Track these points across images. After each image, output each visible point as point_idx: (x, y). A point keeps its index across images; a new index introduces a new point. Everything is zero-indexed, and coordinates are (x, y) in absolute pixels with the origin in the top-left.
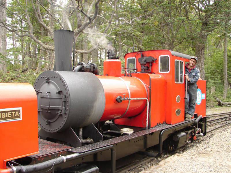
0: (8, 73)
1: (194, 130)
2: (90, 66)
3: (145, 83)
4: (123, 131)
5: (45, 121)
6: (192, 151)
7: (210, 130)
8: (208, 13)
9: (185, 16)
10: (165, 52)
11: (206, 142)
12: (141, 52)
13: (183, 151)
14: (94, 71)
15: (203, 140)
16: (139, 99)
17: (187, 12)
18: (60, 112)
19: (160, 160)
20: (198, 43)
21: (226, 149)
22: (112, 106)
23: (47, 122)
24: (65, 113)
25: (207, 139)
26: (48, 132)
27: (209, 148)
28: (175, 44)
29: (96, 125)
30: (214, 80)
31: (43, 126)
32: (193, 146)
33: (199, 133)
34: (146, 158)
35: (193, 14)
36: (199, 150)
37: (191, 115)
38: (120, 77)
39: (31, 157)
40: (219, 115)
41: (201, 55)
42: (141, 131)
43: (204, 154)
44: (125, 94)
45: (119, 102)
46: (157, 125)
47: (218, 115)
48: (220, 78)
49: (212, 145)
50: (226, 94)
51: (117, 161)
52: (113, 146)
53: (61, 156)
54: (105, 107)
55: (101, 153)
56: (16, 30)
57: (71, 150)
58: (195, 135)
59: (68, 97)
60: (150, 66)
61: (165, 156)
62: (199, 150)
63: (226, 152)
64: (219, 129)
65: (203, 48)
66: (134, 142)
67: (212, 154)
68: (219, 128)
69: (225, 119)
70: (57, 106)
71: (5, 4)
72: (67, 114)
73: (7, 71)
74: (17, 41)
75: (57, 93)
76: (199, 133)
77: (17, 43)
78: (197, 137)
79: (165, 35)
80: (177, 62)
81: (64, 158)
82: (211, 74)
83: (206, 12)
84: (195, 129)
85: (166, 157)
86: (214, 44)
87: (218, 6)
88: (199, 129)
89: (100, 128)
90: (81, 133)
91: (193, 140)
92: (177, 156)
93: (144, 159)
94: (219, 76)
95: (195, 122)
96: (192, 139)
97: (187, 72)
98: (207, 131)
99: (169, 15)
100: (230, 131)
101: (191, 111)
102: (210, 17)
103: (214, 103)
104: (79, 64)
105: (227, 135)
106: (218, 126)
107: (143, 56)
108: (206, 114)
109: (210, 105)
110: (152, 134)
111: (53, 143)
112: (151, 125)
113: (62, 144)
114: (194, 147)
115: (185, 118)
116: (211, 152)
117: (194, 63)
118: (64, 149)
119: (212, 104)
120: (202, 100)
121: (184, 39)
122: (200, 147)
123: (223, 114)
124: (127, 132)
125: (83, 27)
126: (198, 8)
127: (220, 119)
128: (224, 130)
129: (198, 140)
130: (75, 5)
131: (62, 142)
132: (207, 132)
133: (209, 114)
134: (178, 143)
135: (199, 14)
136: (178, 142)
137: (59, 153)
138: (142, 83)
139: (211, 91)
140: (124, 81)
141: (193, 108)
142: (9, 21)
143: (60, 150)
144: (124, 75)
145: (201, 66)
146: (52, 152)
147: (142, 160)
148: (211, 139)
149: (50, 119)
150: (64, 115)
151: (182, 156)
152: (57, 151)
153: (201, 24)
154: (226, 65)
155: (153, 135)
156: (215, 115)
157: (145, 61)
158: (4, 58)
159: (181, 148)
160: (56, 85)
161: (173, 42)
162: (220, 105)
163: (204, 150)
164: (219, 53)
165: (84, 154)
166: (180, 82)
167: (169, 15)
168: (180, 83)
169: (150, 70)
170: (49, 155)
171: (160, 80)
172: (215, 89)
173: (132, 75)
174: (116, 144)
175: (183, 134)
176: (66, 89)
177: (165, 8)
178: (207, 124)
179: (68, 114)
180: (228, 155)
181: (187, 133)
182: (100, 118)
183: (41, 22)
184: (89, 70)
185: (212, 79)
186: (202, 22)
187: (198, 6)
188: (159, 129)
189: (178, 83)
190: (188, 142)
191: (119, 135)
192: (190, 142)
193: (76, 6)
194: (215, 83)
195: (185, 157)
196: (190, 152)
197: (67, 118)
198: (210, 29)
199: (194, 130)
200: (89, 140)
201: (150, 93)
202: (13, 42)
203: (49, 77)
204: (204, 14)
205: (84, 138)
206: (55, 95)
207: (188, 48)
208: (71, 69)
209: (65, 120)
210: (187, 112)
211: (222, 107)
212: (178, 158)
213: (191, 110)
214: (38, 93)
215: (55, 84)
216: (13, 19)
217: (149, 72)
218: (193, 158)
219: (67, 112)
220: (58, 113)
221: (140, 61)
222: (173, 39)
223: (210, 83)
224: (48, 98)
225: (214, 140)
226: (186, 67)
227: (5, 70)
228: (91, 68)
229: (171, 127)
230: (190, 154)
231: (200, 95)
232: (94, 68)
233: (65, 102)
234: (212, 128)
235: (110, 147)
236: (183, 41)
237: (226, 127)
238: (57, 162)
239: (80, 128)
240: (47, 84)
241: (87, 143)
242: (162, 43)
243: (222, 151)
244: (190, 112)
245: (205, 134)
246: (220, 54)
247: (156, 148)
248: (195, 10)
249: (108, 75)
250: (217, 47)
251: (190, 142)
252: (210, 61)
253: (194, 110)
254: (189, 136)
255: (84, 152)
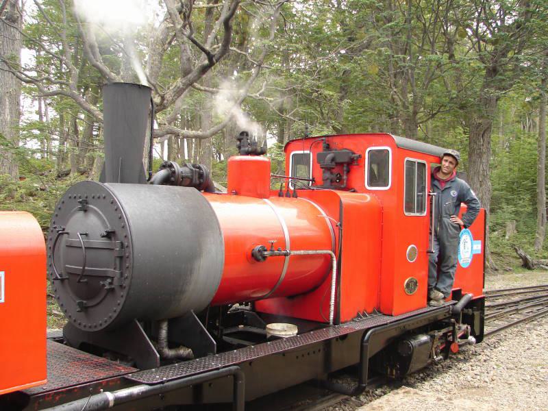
0: (22, 181)
1: (451, 328)
2: (192, 170)
3: (329, 213)
4: (272, 330)
5: (75, 301)
6: (445, 380)
7: (496, 328)
8: (500, 48)
9: (446, 52)
10: (380, 140)
11: (483, 358)
12: (324, 138)
13: (424, 379)
14: (200, 184)
15: (475, 354)
16: (311, 252)
17: (450, 43)
18: (110, 284)
19: (365, 400)
20: (475, 116)
21: (529, 377)
22: (241, 269)
23: (80, 304)
24: (121, 286)
25: (485, 351)
26: (83, 329)
27: (488, 373)
28: (420, 118)
29: (201, 315)
30: (515, 205)
31: (70, 314)
32: (450, 367)
33: (464, 337)
34: (329, 397)
35: (465, 50)
36: (462, 378)
37: (442, 292)
38: (266, 200)
39: (29, 393)
40: (522, 291)
41: (483, 145)
42: (316, 332)
43: (474, 390)
44: (275, 241)
45: (258, 260)
46: (358, 316)
47: (518, 291)
48: (530, 200)
49: (495, 367)
50: (541, 239)
51: (247, 404)
52: (238, 369)
53: (102, 390)
54: (222, 273)
55: (210, 385)
56: (37, 81)
57: (132, 376)
58: (453, 341)
59: (127, 247)
60: (345, 172)
61: (378, 392)
62: (462, 378)
63: (527, 385)
64: (517, 327)
65: (488, 129)
66: (297, 357)
67: (492, 389)
68: (518, 325)
69: (536, 302)
70: (104, 267)
71: (20, 19)
72: (125, 287)
73: (19, 176)
74: (49, 104)
75: (103, 237)
76: (464, 337)
77: (50, 109)
78: (460, 346)
79: (395, 97)
80: (411, 164)
81: (110, 396)
82: (507, 191)
83: (494, 43)
84: (454, 328)
85: (380, 393)
86: (518, 119)
87: (523, 29)
88: (464, 327)
89: (217, 321)
90: (164, 333)
91: (450, 353)
92: (404, 393)
93: (324, 399)
94: (528, 197)
95: (453, 309)
96: (447, 352)
97: (435, 188)
98: (487, 330)
99: (406, 49)
100: (543, 332)
101: (444, 284)
102: (504, 55)
103: (512, 260)
104: (164, 167)
105: (536, 342)
106: (516, 318)
107: (328, 148)
108: (484, 290)
109: (502, 266)
110: (344, 337)
111: (94, 356)
112: (342, 318)
113: (116, 360)
114: (453, 371)
115: (429, 299)
116: (491, 386)
117: (451, 166)
118: (116, 373)
119: (508, 264)
120: (475, 257)
121: (441, 107)
122: (467, 371)
123: (532, 290)
124: (282, 334)
125: (195, 75)
126: (476, 33)
127: (521, 301)
128: (529, 329)
129: (464, 352)
130: (176, 21)
131: (118, 355)
132: (485, 333)
133: (498, 289)
134: (410, 362)
135: (479, 47)
136: (410, 357)
137: (101, 383)
138: (321, 214)
139: (505, 233)
140: (273, 205)
141: (450, 277)
142: (27, 57)
143: (105, 376)
144: (278, 194)
145: (481, 172)
146: (82, 381)
147: (320, 400)
148: (494, 350)
149: (87, 299)
150: (117, 290)
151: (416, 393)
152: (96, 378)
153: (484, 72)
154: (544, 171)
155: (345, 341)
156: (512, 292)
157: (333, 160)
158: (12, 145)
159: (419, 371)
160: (103, 215)
161: (415, 113)
162: (527, 265)
163: (475, 380)
164: (529, 140)
165: (161, 388)
166: (417, 212)
167: (406, 49)
168: (418, 214)
169: (345, 182)
170: (89, 385)
171: (368, 206)
172: (516, 227)
173: (298, 195)
174: (250, 362)
175: (424, 338)
176: (123, 227)
177: (398, 33)
178: (486, 313)
179: (127, 288)
180: (531, 393)
181: (433, 337)
182: (212, 298)
183: (97, 61)
184: (188, 181)
185: (508, 202)
186: (486, 67)
187: (477, 29)
188: (359, 326)
189: (412, 214)
190: (435, 357)
191: (262, 339)
192: (441, 357)
193: (179, 24)
194: (517, 213)
195: (423, 398)
196: (441, 383)
197: (124, 298)
198: (503, 83)
199: (451, 328)
200: (184, 352)
201: (340, 237)
202: (40, 108)
203: (87, 197)
204: (490, 48)
205: (172, 345)
206: (98, 241)
207: (454, 128)
208: (143, 178)
209: (121, 301)
210: (434, 285)
211: (530, 272)
212: (406, 399)
213: (444, 280)
214: (62, 234)
215: (99, 214)
216: (43, 53)
217: (342, 186)
218: (441, 400)
219: (126, 283)
220: (104, 285)
221: (320, 158)
222: (415, 107)
223: (504, 212)
224: (81, 247)
225: (503, 353)
226: (433, 177)
227: (14, 174)
228: (192, 176)
229: (390, 323)
230: (439, 388)
231: (469, 245)
232: (201, 176)
233: (121, 258)
234: (501, 323)
235: (230, 370)
236: (438, 111)
237: (535, 322)
238: (90, 407)
239: (163, 321)
240: (81, 214)
241: (180, 359)
242: (391, 116)
243: (517, 383)
244: (440, 286)
245: (479, 339)
246: (530, 143)
247: (353, 371)
248: (469, 38)
249: (237, 193)
250: (524, 127)
251: (441, 357)
252: (506, 160)
253: (452, 281)
254: (439, 344)
255: (162, 383)
